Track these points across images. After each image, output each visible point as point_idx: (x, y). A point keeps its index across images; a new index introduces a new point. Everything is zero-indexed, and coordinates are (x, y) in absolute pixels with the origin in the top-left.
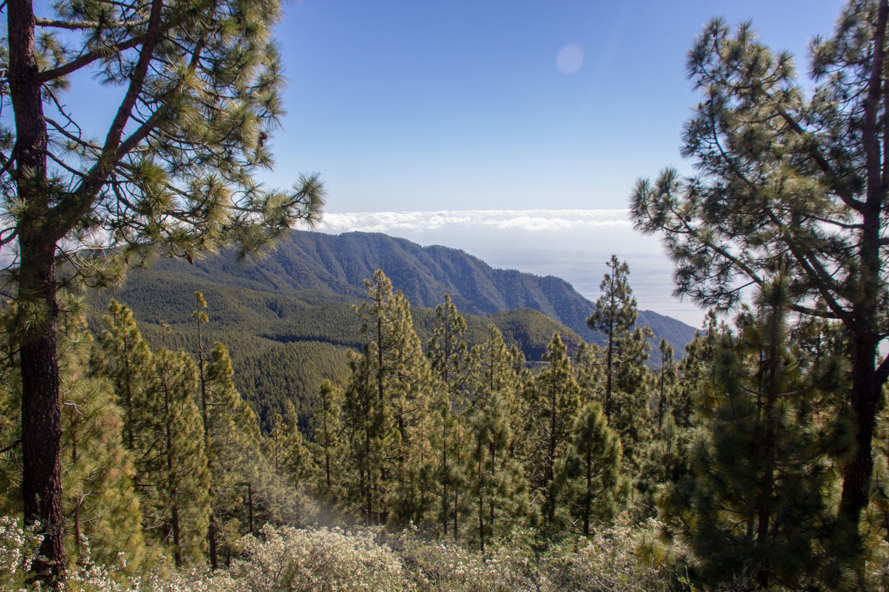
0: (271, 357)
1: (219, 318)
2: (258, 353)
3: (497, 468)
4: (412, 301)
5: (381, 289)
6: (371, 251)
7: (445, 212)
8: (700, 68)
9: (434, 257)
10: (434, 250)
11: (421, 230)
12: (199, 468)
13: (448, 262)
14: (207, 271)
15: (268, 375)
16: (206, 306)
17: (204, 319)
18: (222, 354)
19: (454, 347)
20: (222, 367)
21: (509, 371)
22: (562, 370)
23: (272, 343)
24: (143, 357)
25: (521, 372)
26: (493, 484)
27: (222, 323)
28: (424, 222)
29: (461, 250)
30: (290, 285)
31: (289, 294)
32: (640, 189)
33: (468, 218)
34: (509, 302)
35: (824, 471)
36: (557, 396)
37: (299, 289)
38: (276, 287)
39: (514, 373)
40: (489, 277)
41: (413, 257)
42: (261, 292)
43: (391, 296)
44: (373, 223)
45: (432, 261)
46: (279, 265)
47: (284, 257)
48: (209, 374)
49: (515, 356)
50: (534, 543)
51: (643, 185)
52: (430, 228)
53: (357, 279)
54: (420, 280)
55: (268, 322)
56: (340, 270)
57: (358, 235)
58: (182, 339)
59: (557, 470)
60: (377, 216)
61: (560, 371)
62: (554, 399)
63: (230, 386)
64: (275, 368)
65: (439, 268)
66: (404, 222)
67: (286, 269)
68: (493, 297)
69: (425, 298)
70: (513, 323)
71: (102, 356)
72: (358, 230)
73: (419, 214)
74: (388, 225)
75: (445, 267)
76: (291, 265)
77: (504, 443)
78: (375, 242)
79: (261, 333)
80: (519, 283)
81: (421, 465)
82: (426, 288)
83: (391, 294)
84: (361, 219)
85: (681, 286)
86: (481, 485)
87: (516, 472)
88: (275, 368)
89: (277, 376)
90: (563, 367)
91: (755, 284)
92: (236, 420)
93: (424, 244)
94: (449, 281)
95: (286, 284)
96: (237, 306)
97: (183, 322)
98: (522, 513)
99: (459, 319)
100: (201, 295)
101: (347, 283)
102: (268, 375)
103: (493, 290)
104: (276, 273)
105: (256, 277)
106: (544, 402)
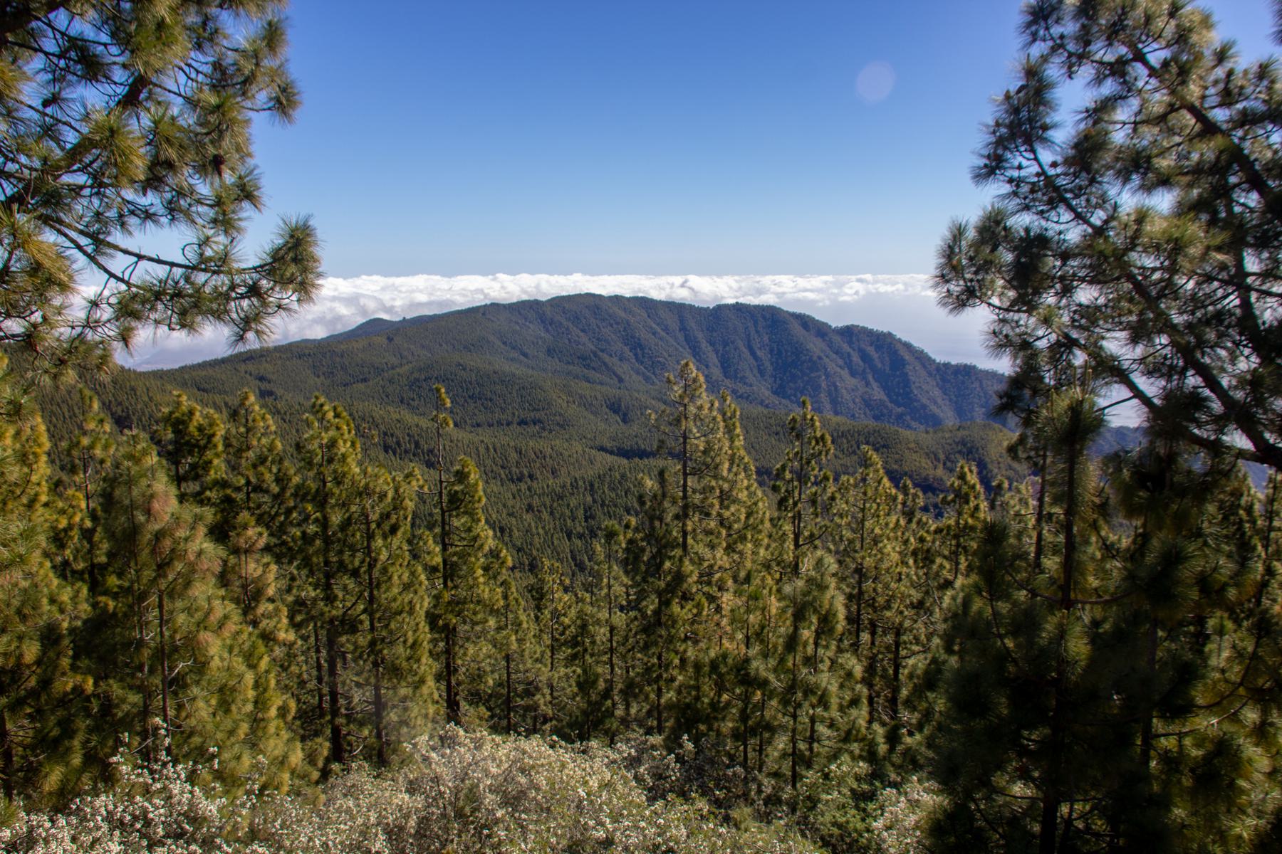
0: (608, 479)
1: (540, 421)
2: (590, 473)
3: (825, 666)
4: (816, 405)
5: (690, 391)
6: (757, 332)
7: (868, 277)
8: (1041, 32)
9: (850, 343)
10: (850, 333)
11: (827, 303)
12: (410, 633)
13: (871, 350)
14: (525, 355)
15: (603, 505)
16: (449, 405)
17: (447, 424)
18: (469, 473)
19: (813, 479)
20: (470, 491)
21: (893, 519)
22: (970, 521)
23: (610, 459)
24: (344, 475)
25: (915, 520)
26: (809, 691)
27: (544, 429)
28: (835, 291)
29: (890, 334)
30: (641, 378)
31: (638, 391)
32: (954, 237)
33: (901, 287)
34: (960, 412)
35: (930, 769)
36: (962, 559)
37: (653, 383)
38: (621, 380)
39: (902, 522)
40: (930, 374)
41: (819, 342)
42: (599, 387)
43: (704, 398)
44: (760, 292)
45: (846, 347)
46: (626, 349)
47: (633, 337)
48: (450, 501)
49: (906, 494)
50: (855, 786)
51: (958, 233)
52: (842, 299)
53: (736, 371)
54: (827, 376)
55: (608, 428)
56: (713, 359)
57: (739, 308)
58: (488, 449)
59: (911, 676)
60: (767, 280)
61: (966, 523)
62: (957, 564)
63: (479, 520)
64: (613, 495)
65: (856, 358)
66: (806, 290)
67: (636, 355)
68: (935, 403)
69: (835, 402)
70: (963, 443)
71: (292, 472)
72: (742, 300)
73: (829, 278)
74: (780, 295)
75: (865, 357)
76: (642, 349)
77: (832, 630)
78: (764, 317)
79: (597, 444)
80: (976, 384)
81: (712, 654)
82: (836, 387)
83: (704, 395)
84: (743, 284)
85: (1004, 400)
86: (795, 693)
87: (849, 675)
88: (613, 495)
89: (616, 506)
90: (972, 516)
91: (1135, 401)
92: (486, 569)
93: (836, 323)
94: (870, 377)
95: (634, 376)
96: (564, 405)
97: (490, 425)
98: (852, 738)
99: (823, 437)
100: (443, 390)
101: (721, 377)
102: (603, 505)
103: (937, 393)
104: (621, 360)
105: (593, 364)
106: (942, 566)
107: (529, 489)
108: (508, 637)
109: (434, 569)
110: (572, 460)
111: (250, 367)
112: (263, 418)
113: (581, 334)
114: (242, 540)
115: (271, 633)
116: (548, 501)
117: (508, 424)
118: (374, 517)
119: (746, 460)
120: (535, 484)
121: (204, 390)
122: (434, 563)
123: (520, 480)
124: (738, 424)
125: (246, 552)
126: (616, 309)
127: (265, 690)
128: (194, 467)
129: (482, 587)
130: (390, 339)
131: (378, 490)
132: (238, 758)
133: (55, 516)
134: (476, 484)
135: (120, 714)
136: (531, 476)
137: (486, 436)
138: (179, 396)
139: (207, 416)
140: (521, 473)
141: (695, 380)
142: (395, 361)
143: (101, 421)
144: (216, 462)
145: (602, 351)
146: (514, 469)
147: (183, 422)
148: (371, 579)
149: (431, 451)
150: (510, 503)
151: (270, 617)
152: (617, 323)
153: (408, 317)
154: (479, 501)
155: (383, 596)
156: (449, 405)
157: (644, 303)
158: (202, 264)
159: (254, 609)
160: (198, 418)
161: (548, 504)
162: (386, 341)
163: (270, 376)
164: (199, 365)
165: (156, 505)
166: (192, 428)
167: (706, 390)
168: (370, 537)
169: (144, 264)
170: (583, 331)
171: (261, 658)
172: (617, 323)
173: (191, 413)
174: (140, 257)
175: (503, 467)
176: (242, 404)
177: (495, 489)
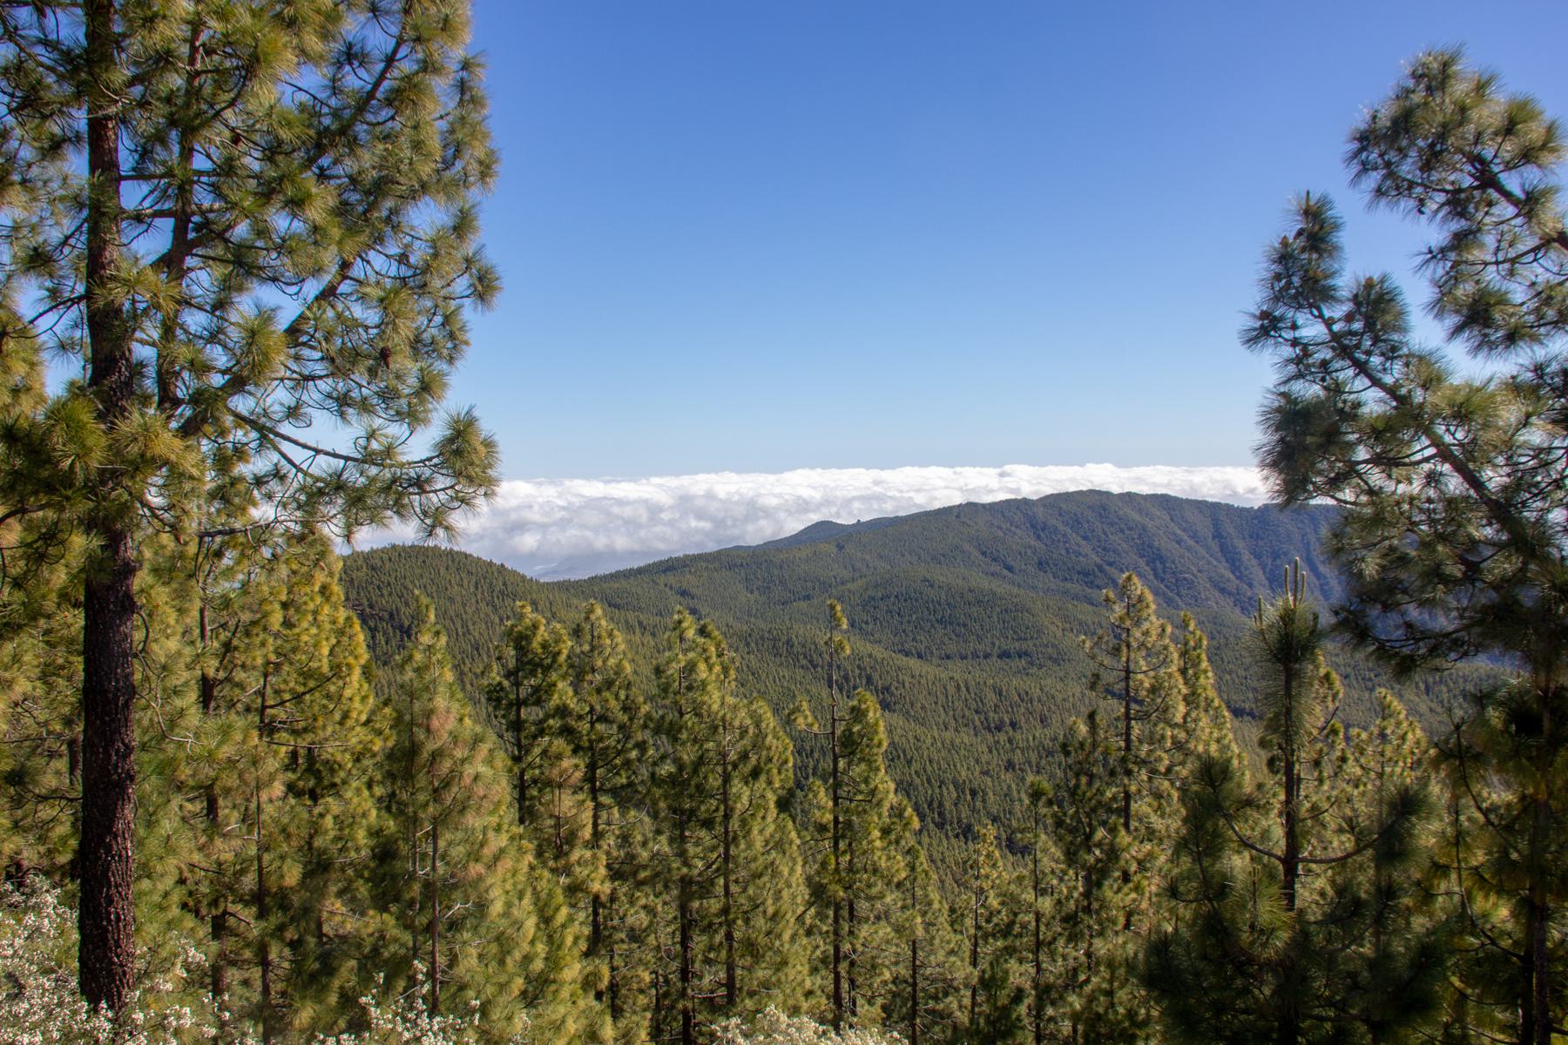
1: (1026, 654)
5: (1135, 608)
12: (770, 902)
14: (1010, 569)
16: (845, 627)
18: (867, 710)
27: (1032, 664)
46: (1142, 563)
47: (1150, 546)
58: (958, 687)
63: (878, 769)
67: (1154, 570)
83: (1153, 618)
92: (886, 832)
96: (1059, 634)
97: (963, 658)
100: (839, 608)
107: (1010, 741)
108: (911, 919)
109: (822, 828)
110: (1068, 705)
111: (671, 579)
112: (611, 635)
113: (1083, 543)
114: (556, 771)
115: (583, 882)
116: (1033, 757)
117: (986, 656)
118: (733, 756)
119: (1216, 703)
120: (1018, 736)
121: (617, 606)
122: (824, 821)
123: (999, 728)
124: (1204, 656)
125: (560, 786)
126: (1129, 511)
127: (559, 947)
128: (537, 689)
129: (879, 853)
130: (840, 547)
131: (737, 723)
132: (509, 1018)
133: (370, 737)
134: (877, 724)
135: (386, 954)
136: (1013, 725)
137: (957, 670)
138: (523, 607)
139: (553, 632)
140: (1002, 721)
141: (1140, 599)
142: (845, 574)
143: (437, 633)
144: (560, 685)
145: (1110, 564)
146: (991, 714)
147: (527, 638)
148: (726, 832)
149: (887, 689)
150: (985, 758)
151: (586, 863)
152: (1130, 529)
153: (863, 520)
154: (880, 745)
155: (740, 850)
156: (845, 627)
157: (1165, 502)
158: (368, 458)
159: (566, 854)
160: (542, 633)
161: (1034, 761)
162: (835, 550)
163: (694, 591)
164: (612, 575)
165: (435, 723)
166: (535, 645)
167: (1156, 612)
168: (727, 779)
169: (321, 457)
170: (1085, 538)
171: (557, 909)
172: (1130, 529)
173: (535, 627)
174: (318, 451)
175: (977, 712)
176: (587, 618)
177: (966, 740)
